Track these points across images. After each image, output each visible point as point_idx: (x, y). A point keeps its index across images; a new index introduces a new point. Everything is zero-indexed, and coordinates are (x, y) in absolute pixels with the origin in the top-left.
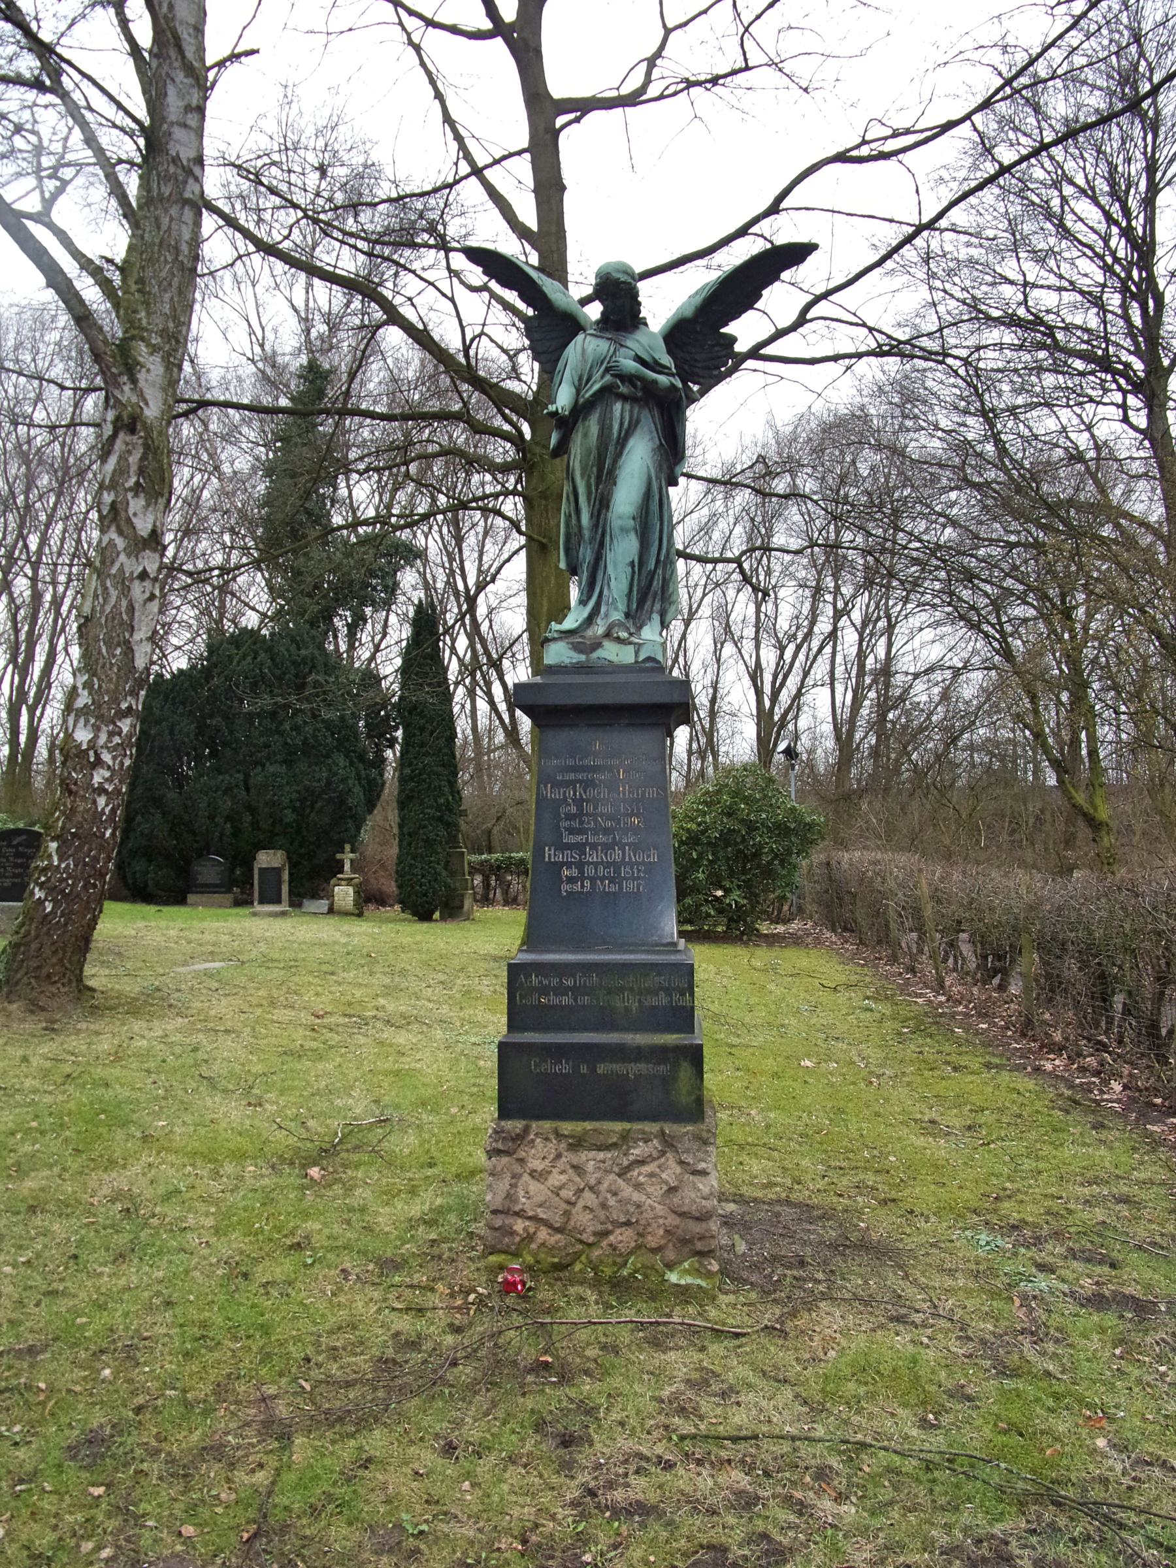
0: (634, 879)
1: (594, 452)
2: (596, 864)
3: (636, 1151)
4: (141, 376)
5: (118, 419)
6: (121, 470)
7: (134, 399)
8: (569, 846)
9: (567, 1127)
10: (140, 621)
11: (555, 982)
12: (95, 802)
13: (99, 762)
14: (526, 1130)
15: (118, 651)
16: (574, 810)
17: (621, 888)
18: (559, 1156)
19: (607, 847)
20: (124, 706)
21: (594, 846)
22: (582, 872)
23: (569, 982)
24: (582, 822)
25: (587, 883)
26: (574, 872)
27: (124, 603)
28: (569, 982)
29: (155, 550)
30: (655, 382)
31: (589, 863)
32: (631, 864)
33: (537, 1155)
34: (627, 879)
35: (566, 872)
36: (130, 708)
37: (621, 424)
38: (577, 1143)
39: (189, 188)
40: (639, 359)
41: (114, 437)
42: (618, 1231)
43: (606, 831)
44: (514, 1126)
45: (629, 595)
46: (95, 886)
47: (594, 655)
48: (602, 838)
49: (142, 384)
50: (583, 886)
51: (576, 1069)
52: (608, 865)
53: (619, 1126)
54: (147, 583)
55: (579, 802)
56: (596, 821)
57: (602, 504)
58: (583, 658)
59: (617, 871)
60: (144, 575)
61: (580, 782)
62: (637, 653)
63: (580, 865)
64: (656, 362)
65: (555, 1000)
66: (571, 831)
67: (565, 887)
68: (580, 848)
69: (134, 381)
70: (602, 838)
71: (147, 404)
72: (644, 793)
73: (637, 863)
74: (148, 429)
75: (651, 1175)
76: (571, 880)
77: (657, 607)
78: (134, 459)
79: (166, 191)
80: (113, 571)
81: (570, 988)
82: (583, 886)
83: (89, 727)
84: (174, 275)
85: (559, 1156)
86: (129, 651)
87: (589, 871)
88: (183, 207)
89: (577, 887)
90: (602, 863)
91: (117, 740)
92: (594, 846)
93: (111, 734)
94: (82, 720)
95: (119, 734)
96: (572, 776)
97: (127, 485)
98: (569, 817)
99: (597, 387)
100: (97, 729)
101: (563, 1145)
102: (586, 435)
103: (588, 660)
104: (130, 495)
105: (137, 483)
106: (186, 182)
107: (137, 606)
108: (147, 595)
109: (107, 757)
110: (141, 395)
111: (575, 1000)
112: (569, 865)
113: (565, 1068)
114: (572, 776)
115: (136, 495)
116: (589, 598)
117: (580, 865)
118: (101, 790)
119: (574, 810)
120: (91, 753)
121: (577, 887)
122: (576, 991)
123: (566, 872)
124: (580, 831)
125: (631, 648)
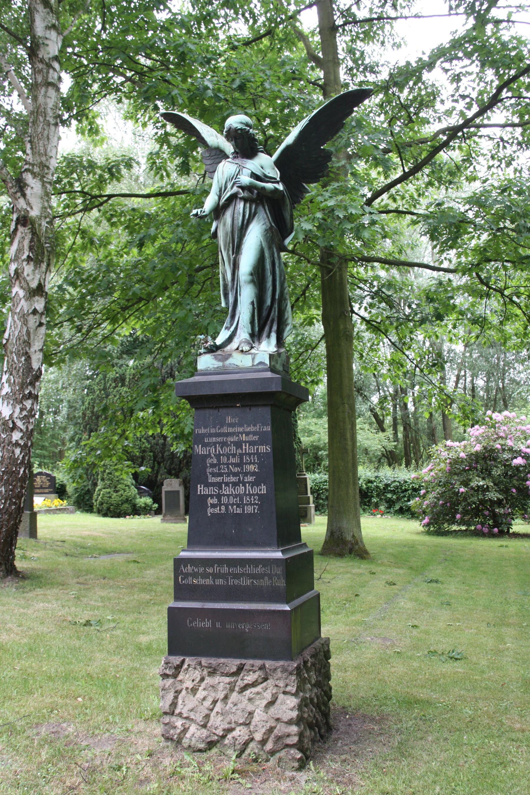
0: (251, 504)
1: (230, 234)
2: (228, 496)
3: (249, 678)
4: (28, 192)
5: (18, 219)
6: (20, 251)
7: (25, 206)
8: (213, 485)
9: (204, 661)
10: (34, 339)
11: (201, 570)
12: (13, 452)
13: (15, 427)
14: (183, 662)
15: (23, 358)
16: (215, 461)
17: (243, 510)
18: (202, 679)
19: (235, 484)
20: (27, 392)
21: (227, 484)
22: (219, 500)
23: (210, 570)
24: (220, 469)
25: (223, 508)
26: (215, 501)
27: (25, 329)
28: (210, 570)
29: (42, 296)
30: (263, 188)
31: (224, 495)
32: (250, 495)
33: (188, 678)
34: (247, 505)
35: (210, 501)
36: (30, 393)
37: (244, 216)
38: (213, 672)
39: (50, 76)
40: (254, 175)
41: (16, 230)
42: (238, 729)
43: (235, 474)
44: (176, 660)
45: (252, 322)
46: (15, 503)
47: (227, 362)
48: (233, 479)
49: (28, 196)
50: (220, 510)
51: (214, 624)
52: (236, 496)
53: (238, 662)
54: (37, 317)
55: (218, 456)
56: (228, 468)
57: (235, 266)
58: (220, 364)
59: (241, 500)
60: (35, 312)
61: (219, 443)
62: (253, 359)
63: (219, 497)
64: (265, 176)
65: (202, 581)
66: (214, 475)
67: (210, 511)
68: (219, 485)
69: (24, 195)
70: (233, 479)
71: (32, 208)
72: (258, 449)
73: (254, 495)
74: (33, 223)
75: (258, 693)
76: (213, 506)
77: (275, 328)
78: (26, 243)
79: (40, 79)
80: (18, 311)
81: (210, 574)
82: (220, 510)
83: (10, 406)
84: (44, 129)
85: (202, 679)
86: (28, 358)
87: (224, 500)
88: (47, 87)
89: (217, 510)
90: (232, 495)
91: (25, 413)
92: (227, 484)
93: (22, 410)
94: (6, 402)
95: (25, 409)
96: (214, 439)
97: (23, 258)
98: (213, 466)
99: (228, 195)
100: (14, 407)
101: (205, 672)
102: (224, 224)
103: (224, 366)
104: (25, 263)
105: (29, 256)
106: (48, 72)
107: (32, 331)
108: (37, 324)
109: (19, 424)
110: (28, 204)
111: (214, 581)
112: (212, 496)
113: (208, 624)
114: (214, 439)
115: (28, 263)
116: (232, 325)
117: (219, 497)
118: (17, 444)
119: (215, 461)
120: (10, 422)
121: (217, 510)
122: (215, 576)
123: (210, 501)
124: (220, 475)
125: (249, 357)
